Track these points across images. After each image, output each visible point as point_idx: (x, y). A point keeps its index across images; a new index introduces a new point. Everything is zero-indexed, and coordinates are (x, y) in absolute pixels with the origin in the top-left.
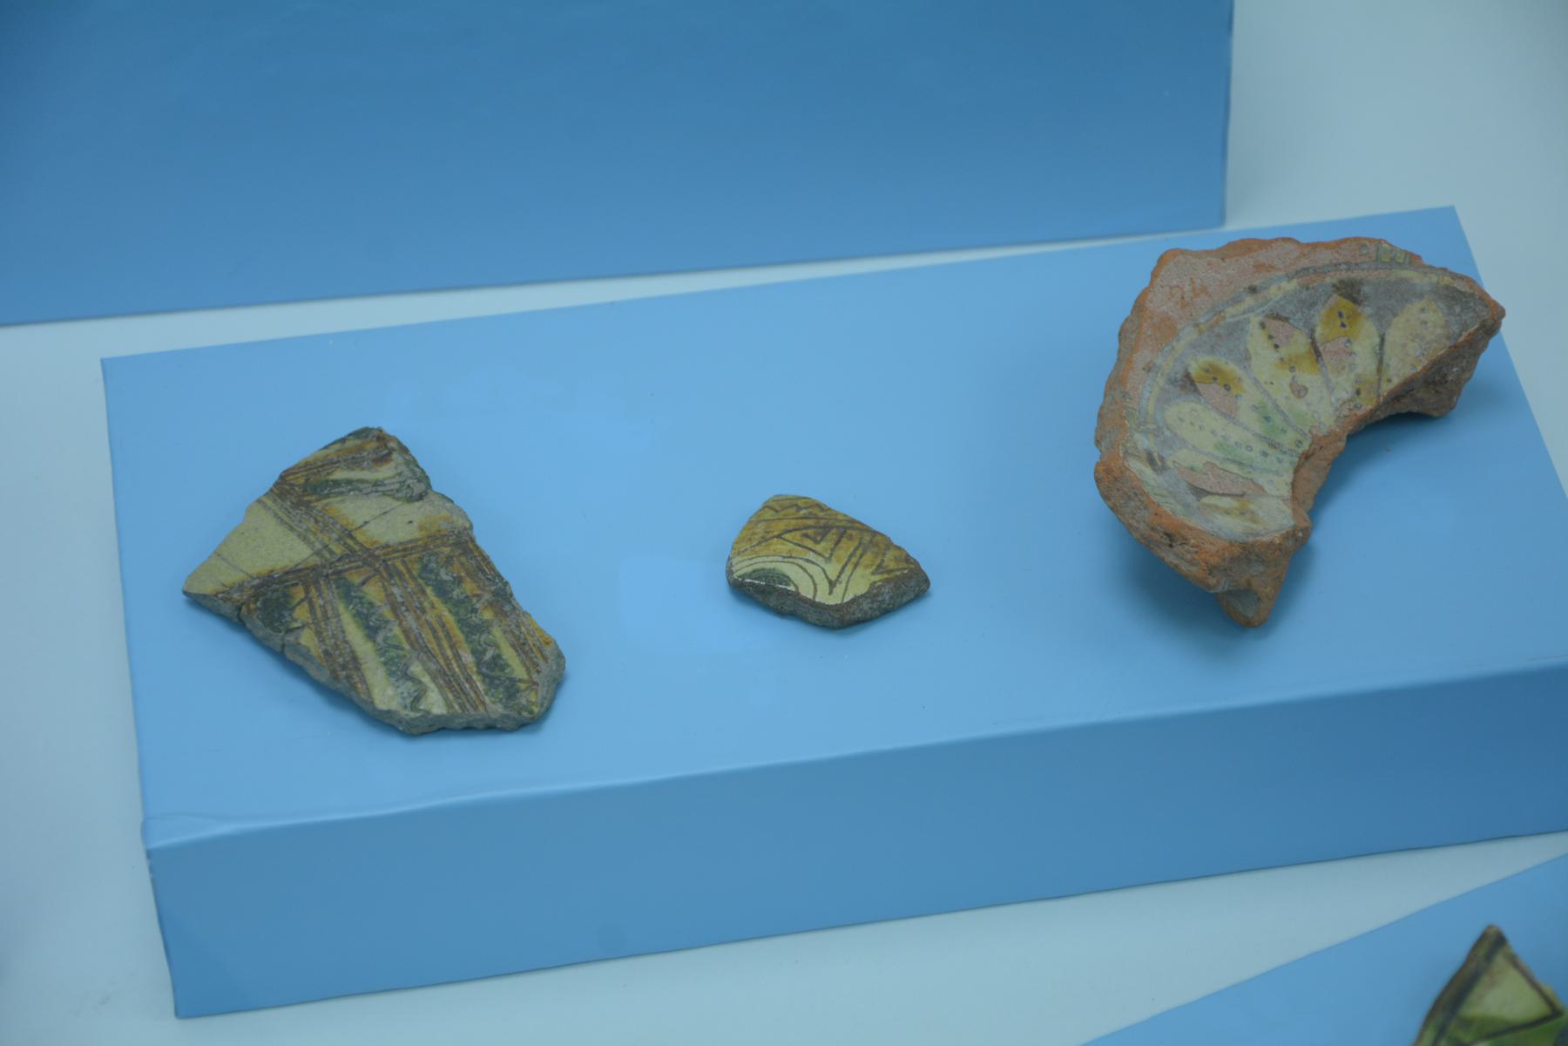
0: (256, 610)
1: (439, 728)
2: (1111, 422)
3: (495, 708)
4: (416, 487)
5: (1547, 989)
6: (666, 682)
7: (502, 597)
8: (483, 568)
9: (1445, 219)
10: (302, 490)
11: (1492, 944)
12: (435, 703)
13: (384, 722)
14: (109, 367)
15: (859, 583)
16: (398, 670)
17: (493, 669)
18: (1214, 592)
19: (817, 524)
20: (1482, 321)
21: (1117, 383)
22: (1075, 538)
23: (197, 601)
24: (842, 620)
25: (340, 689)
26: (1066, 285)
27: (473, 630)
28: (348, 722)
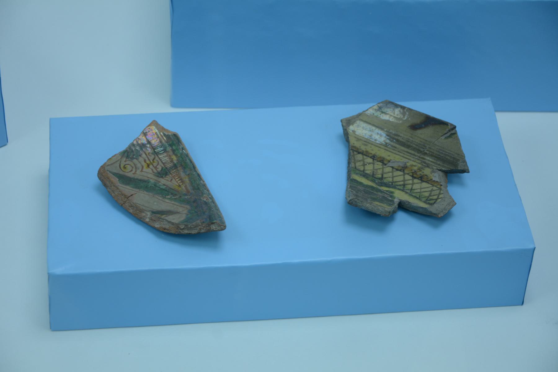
12: (360, 157)
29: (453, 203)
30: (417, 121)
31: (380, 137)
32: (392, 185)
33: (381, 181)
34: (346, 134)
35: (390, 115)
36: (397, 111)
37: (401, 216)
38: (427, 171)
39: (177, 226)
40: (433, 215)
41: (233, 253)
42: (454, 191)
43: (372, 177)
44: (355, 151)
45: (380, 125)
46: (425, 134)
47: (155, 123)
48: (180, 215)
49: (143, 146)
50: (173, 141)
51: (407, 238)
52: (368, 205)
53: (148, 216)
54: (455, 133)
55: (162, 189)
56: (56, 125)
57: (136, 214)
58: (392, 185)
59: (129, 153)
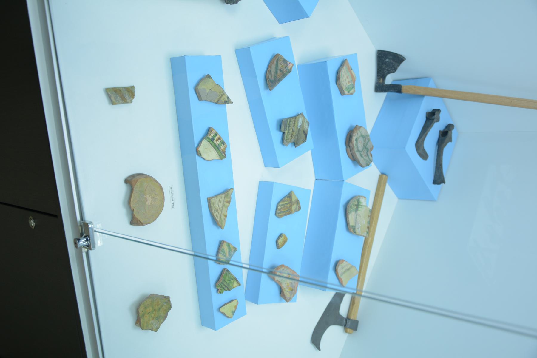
0: (290, 196)
1: (277, 207)
2: (287, 267)
3: (278, 212)
4: (296, 211)
5: (419, 80)
6: (277, 226)
7: (286, 215)
8: (288, 214)
9: (295, 301)
10: (298, 202)
11: (240, 285)
12: (279, 207)
13: (279, 203)
14: (310, 190)
15: (279, 243)
16: (282, 205)
17: (281, 212)
18: (272, 272)
19: (285, 241)
20: (287, 300)
21: (290, 269)
22: (278, 263)
23: (291, 192)
24: (277, 241)
25: (282, 200)
26: (297, 268)
27: (284, 212)
28: (279, 200)
29: (287, 146)
30: (306, 132)
31: (300, 124)
32: (289, 130)
33: (289, 127)
34: (299, 115)
35: (306, 125)
36: (307, 126)
37: (281, 133)
38: (293, 137)
39: (268, 78)
40: (283, 141)
41: (264, 93)
42: (290, 145)
43: (290, 124)
44: (295, 118)
45: (303, 123)
46: (303, 135)
47: (293, 65)
48: (272, 78)
49: (287, 63)
50: (289, 71)
51: (277, 136)
52: (282, 125)
53: (269, 70)
54: (225, 290)
55: (276, 71)
56: (287, 38)
57: (269, 66)
58: (289, 130)
59: (285, 61)
